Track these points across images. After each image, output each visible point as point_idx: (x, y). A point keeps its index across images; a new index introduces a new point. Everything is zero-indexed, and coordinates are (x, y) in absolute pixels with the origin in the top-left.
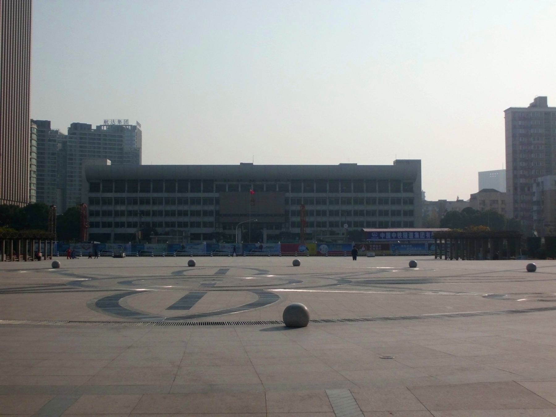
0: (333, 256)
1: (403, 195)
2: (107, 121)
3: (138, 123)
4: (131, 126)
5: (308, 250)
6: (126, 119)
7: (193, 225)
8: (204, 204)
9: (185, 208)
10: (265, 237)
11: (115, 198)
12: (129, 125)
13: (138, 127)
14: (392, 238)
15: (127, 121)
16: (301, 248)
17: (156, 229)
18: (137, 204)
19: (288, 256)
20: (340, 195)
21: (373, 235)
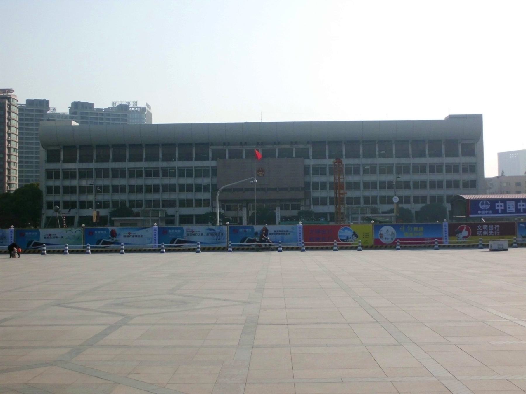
0: (410, 248)
1: (462, 160)
2: (116, 103)
3: (147, 105)
4: (140, 107)
5: (357, 236)
6: (136, 100)
7: (182, 203)
8: (196, 176)
9: (173, 181)
10: (278, 219)
11: (79, 169)
12: (138, 107)
13: (147, 109)
14: (518, 211)
15: (136, 102)
16: (343, 233)
17: (133, 209)
18: (108, 177)
19: (317, 249)
20: (379, 161)
21: (481, 207)
